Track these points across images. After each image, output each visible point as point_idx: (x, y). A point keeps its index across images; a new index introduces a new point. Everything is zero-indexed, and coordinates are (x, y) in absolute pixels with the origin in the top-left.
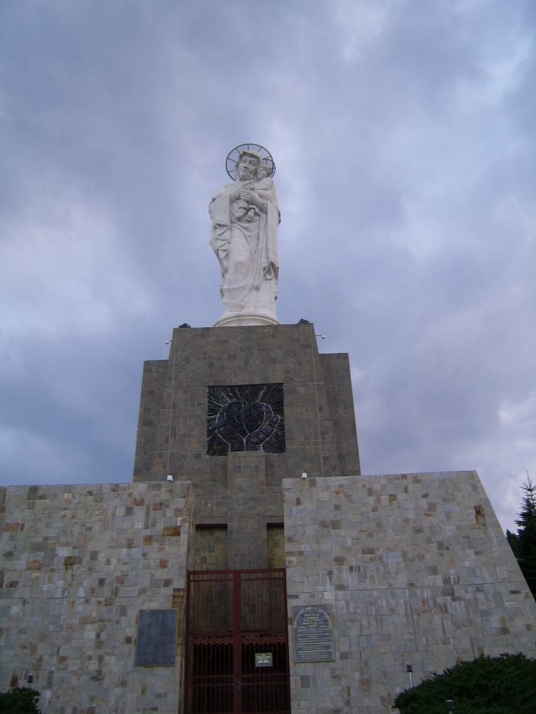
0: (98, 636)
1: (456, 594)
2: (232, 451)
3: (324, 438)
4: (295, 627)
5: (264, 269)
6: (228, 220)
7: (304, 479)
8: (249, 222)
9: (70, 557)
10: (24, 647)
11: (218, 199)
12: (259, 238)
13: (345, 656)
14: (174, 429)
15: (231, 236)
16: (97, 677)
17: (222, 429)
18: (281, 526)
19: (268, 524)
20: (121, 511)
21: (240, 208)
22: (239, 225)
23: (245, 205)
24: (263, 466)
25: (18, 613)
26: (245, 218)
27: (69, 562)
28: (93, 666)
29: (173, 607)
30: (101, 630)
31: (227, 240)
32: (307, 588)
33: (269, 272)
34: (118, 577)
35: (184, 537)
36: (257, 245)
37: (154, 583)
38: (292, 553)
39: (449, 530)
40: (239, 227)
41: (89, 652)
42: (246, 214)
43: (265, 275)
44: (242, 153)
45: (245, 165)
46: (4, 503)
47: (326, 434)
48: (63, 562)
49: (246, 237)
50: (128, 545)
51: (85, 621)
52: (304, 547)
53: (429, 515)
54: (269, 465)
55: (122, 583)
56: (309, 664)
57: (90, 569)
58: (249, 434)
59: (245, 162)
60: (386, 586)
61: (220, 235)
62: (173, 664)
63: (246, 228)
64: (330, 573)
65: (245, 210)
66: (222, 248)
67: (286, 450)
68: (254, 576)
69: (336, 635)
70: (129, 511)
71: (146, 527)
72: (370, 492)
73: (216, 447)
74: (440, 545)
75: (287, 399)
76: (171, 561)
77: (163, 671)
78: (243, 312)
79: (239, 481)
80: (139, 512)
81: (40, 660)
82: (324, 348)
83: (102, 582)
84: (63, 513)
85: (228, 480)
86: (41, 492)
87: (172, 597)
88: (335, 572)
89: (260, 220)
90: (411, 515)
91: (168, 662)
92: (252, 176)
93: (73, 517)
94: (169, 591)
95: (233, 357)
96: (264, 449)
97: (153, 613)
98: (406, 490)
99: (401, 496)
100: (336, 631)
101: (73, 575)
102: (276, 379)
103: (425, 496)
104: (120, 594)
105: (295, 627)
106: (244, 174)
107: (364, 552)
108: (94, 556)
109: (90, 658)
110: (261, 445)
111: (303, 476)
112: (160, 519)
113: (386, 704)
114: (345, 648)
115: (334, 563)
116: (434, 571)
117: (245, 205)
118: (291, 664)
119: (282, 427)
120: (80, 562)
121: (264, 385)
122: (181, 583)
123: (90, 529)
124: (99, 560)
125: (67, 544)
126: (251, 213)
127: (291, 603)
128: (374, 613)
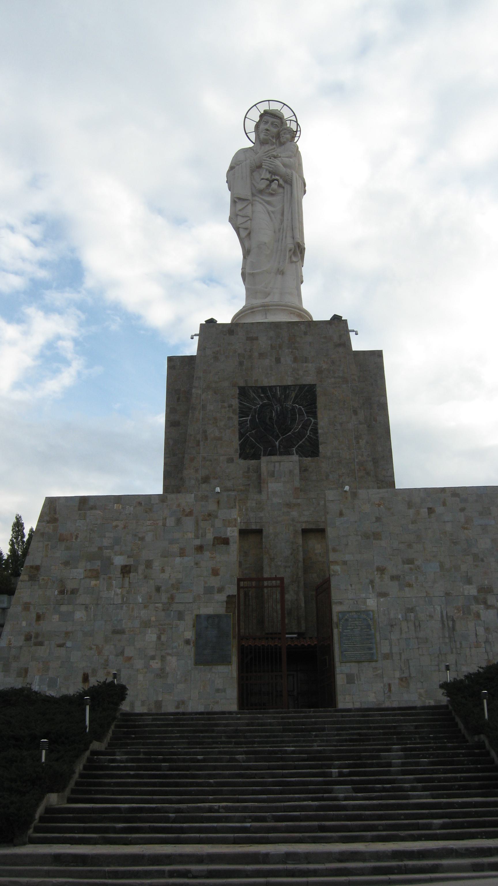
0: (159, 638)
1: (489, 603)
2: (263, 456)
3: (358, 442)
4: (341, 630)
5: (290, 250)
6: (250, 194)
7: (346, 491)
8: (272, 195)
9: (126, 566)
10: (91, 649)
11: (237, 167)
12: (283, 214)
13: (387, 656)
14: (205, 432)
15: (253, 212)
16: (162, 674)
17: (253, 432)
18: (321, 532)
19: (302, 529)
20: (171, 522)
21: (263, 179)
23: (268, 176)
24: (297, 471)
25: (82, 618)
26: (267, 191)
27: (126, 570)
28: (156, 665)
29: (227, 611)
30: (161, 633)
31: (249, 217)
32: (347, 597)
33: (295, 253)
34: (173, 585)
35: (234, 547)
36: (282, 221)
37: (209, 590)
38: (336, 563)
40: (262, 201)
41: (152, 653)
42: (269, 185)
43: (291, 257)
44: (262, 112)
45: (266, 127)
46: (55, 513)
48: (120, 570)
49: (269, 213)
50: (180, 554)
51: (146, 624)
52: (348, 557)
53: (466, 529)
54: (304, 470)
55: (178, 589)
56: (353, 664)
57: (146, 577)
58: (281, 438)
59: (267, 123)
60: (425, 595)
61: (240, 210)
62: (229, 663)
63: (268, 203)
64: (372, 582)
65: (268, 182)
66: (243, 226)
67: (320, 454)
69: (378, 639)
70: (178, 521)
71: (197, 537)
72: (410, 505)
73: (249, 450)
74: (476, 557)
75: (321, 401)
77: (221, 668)
78: (268, 300)
79: (273, 486)
80: (189, 523)
81: (107, 661)
82: (358, 344)
83: (158, 589)
84: (114, 523)
85: (262, 485)
87: (225, 603)
88: (377, 580)
89: (284, 193)
90: (448, 527)
91: (225, 661)
92: (274, 141)
93: (125, 527)
94: (222, 597)
95: (262, 355)
96: (297, 453)
97: (209, 617)
98: (444, 504)
99: (439, 509)
100: (378, 634)
101: (129, 582)
102: (309, 380)
103: (462, 510)
104: (176, 600)
105: (341, 630)
106: (265, 137)
107: (404, 563)
108: (149, 564)
109: (153, 658)
110: (294, 449)
111: (345, 489)
112: (209, 529)
113: (423, 699)
114: (385, 649)
115: (376, 573)
116: (469, 581)
117: (268, 176)
118: (337, 664)
119: (315, 431)
120: (136, 571)
121: (295, 386)
122: (232, 590)
123: (142, 539)
124: (153, 568)
125: (121, 554)
126: (274, 185)
127: (336, 609)
128: (412, 618)
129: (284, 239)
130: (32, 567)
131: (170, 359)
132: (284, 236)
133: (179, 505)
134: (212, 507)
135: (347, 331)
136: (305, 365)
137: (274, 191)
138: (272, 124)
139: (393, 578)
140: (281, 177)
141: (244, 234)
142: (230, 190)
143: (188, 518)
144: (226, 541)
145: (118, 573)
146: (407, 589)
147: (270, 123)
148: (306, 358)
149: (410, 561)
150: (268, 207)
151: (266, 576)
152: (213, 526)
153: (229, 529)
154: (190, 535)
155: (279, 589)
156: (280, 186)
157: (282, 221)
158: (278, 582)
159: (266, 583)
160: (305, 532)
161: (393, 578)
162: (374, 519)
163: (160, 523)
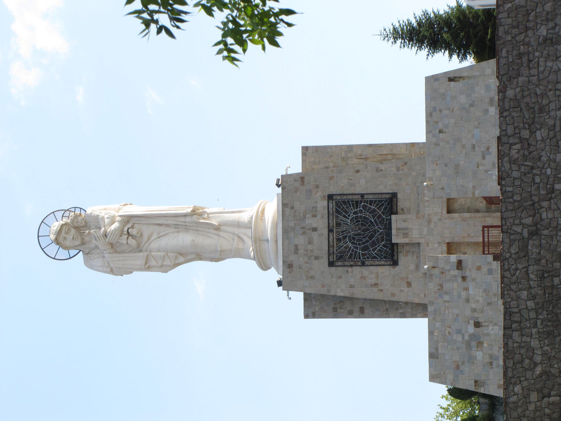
12: (160, 225)
14: (371, 285)
20: (447, 298)
22: (144, 245)
27: (477, 325)
36: (167, 225)
39: (463, 99)
40: (147, 244)
47: (378, 168)
49: (159, 237)
52: (470, 185)
53: (453, 110)
59: (65, 238)
64: (486, 171)
65: (130, 237)
68: (486, 235)
70: (446, 293)
72: (437, 144)
74: (472, 105)
76: (478, 264)
83: (489, 304)
86: (434, 351)
98: (437, 122)
99: (440, 126)
108: (474, 310)
116: (487, 111)
120: (478, 318)
123: (457, 315)
129: (187, 224)
130: (475, 386)
131: (306, 316)
132: (184, 224)
133: (435, 293)
134: (436, 271)
135: (287, 175)
136: (318, 209)
137: (138, 233)
138: (66, 233)
139: (484, 158)
140: (125, 226)
141: (181, 259)
142: (131, 272)
143: (444, 286)
144: (460, 262)
145: (478, 329)
146: (490, 150)
147: (66, 236)
148: (313, 208)
149: (473, 147)
150: (153, 238)
151: (481, 240)
152: (449, 270)
153: (451, 260)
154: (455, 285)
155: (490, 229)
156: (132, 227)
157: (167, 225)
158: (486, 229)
159: (486, 240)
160: (449, 212)
161: (484, 158)
162: (446, 168)
163: (447, 304)
